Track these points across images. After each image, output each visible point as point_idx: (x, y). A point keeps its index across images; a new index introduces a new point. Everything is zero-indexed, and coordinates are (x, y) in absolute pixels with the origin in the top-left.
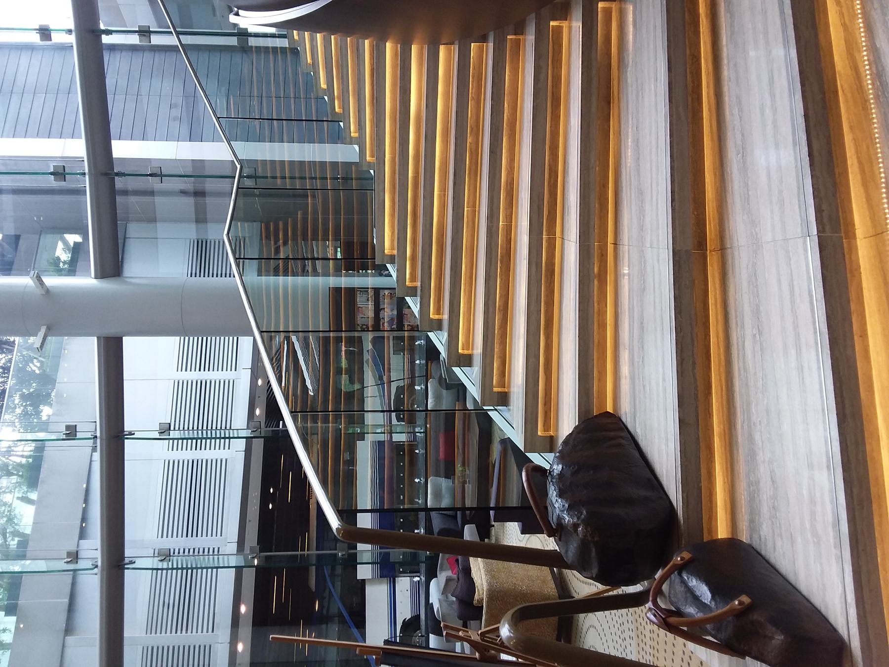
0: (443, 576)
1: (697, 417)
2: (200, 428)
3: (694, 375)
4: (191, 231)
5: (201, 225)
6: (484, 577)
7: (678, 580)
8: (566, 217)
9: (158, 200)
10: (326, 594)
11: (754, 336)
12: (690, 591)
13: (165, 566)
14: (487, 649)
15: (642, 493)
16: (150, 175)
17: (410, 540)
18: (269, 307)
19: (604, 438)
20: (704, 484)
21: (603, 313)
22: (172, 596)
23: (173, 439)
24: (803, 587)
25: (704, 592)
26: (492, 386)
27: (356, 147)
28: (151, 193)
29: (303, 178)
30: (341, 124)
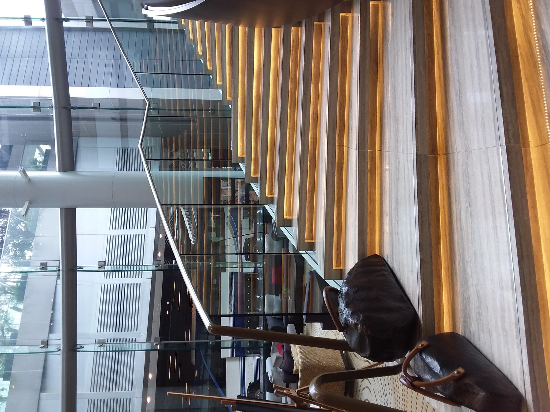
0: (274, 356)
1: (431, 257)
2: (124, 264)
3: (429, 232)
4: (118, 143)
5: (125, 139)
6: (299, 356)
7: (419, 358)
8: (350, 134)
9: (98, 123)
10: (202, 367)
11: (467, 207)
12: (427, 365)
13: (102, 350)
14: (301, 401)
15: (397, 304)
16: (93, 108)
17: (254, 334)
18: (166, 190)
19: (374, 270)
20: (435, 299)
21: (373, 193)
22: (107, 368)
23: (107, 271)
24: (497, 363)
25: (436, 366)
26: (304, 238)
27: (221, 91)
28: (94, 119)
29: (187, 110)
30: (211, 76)
